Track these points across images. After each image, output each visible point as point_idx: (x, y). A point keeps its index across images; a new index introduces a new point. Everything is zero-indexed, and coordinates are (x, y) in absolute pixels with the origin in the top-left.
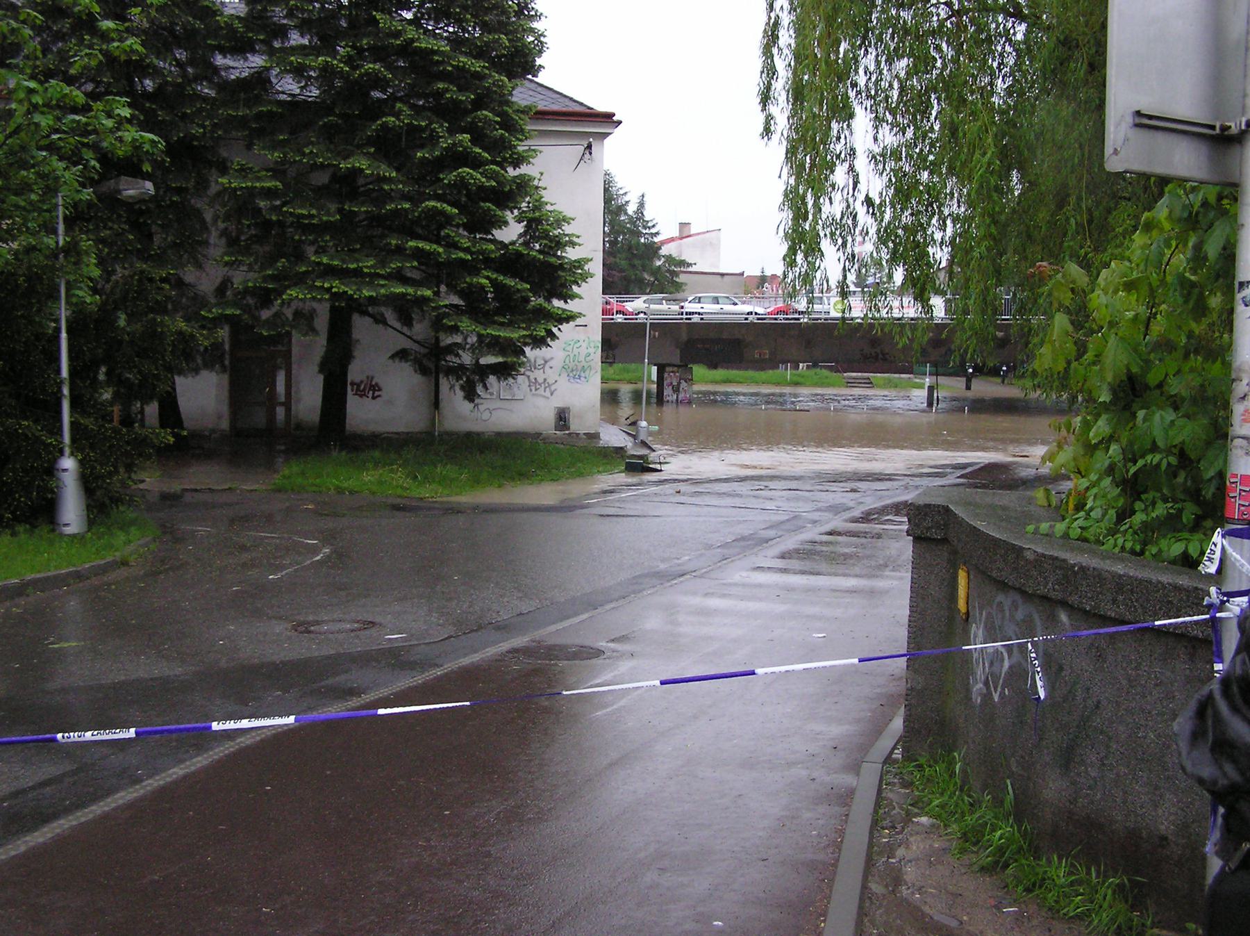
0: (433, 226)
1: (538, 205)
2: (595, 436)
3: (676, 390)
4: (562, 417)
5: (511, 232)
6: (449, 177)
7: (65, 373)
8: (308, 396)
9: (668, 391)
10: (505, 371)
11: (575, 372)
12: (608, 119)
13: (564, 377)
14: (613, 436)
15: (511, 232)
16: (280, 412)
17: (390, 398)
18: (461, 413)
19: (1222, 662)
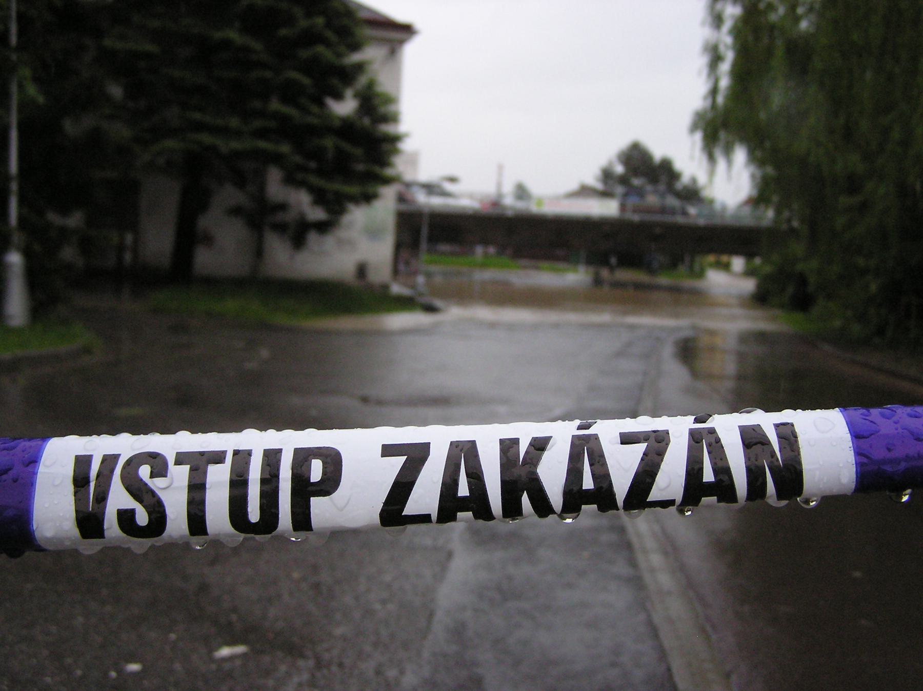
0: (290, 93)
1: (371, 85)
2: (385, 287)
3: (407, 263)
4: (362, 270)
5: (345, 107)
6: (304, 54)
7: (14, 166)
8: (157, 241)
9: (402, 267)
10: (323, 227)
11: (373, 233)
12: (407, 30)
13: (363, 240)
14: (397, 289)
15: (345, 107)
16: (128, 257)
17: (225, 247)
18: (283, 259)
19: (152, 476)
